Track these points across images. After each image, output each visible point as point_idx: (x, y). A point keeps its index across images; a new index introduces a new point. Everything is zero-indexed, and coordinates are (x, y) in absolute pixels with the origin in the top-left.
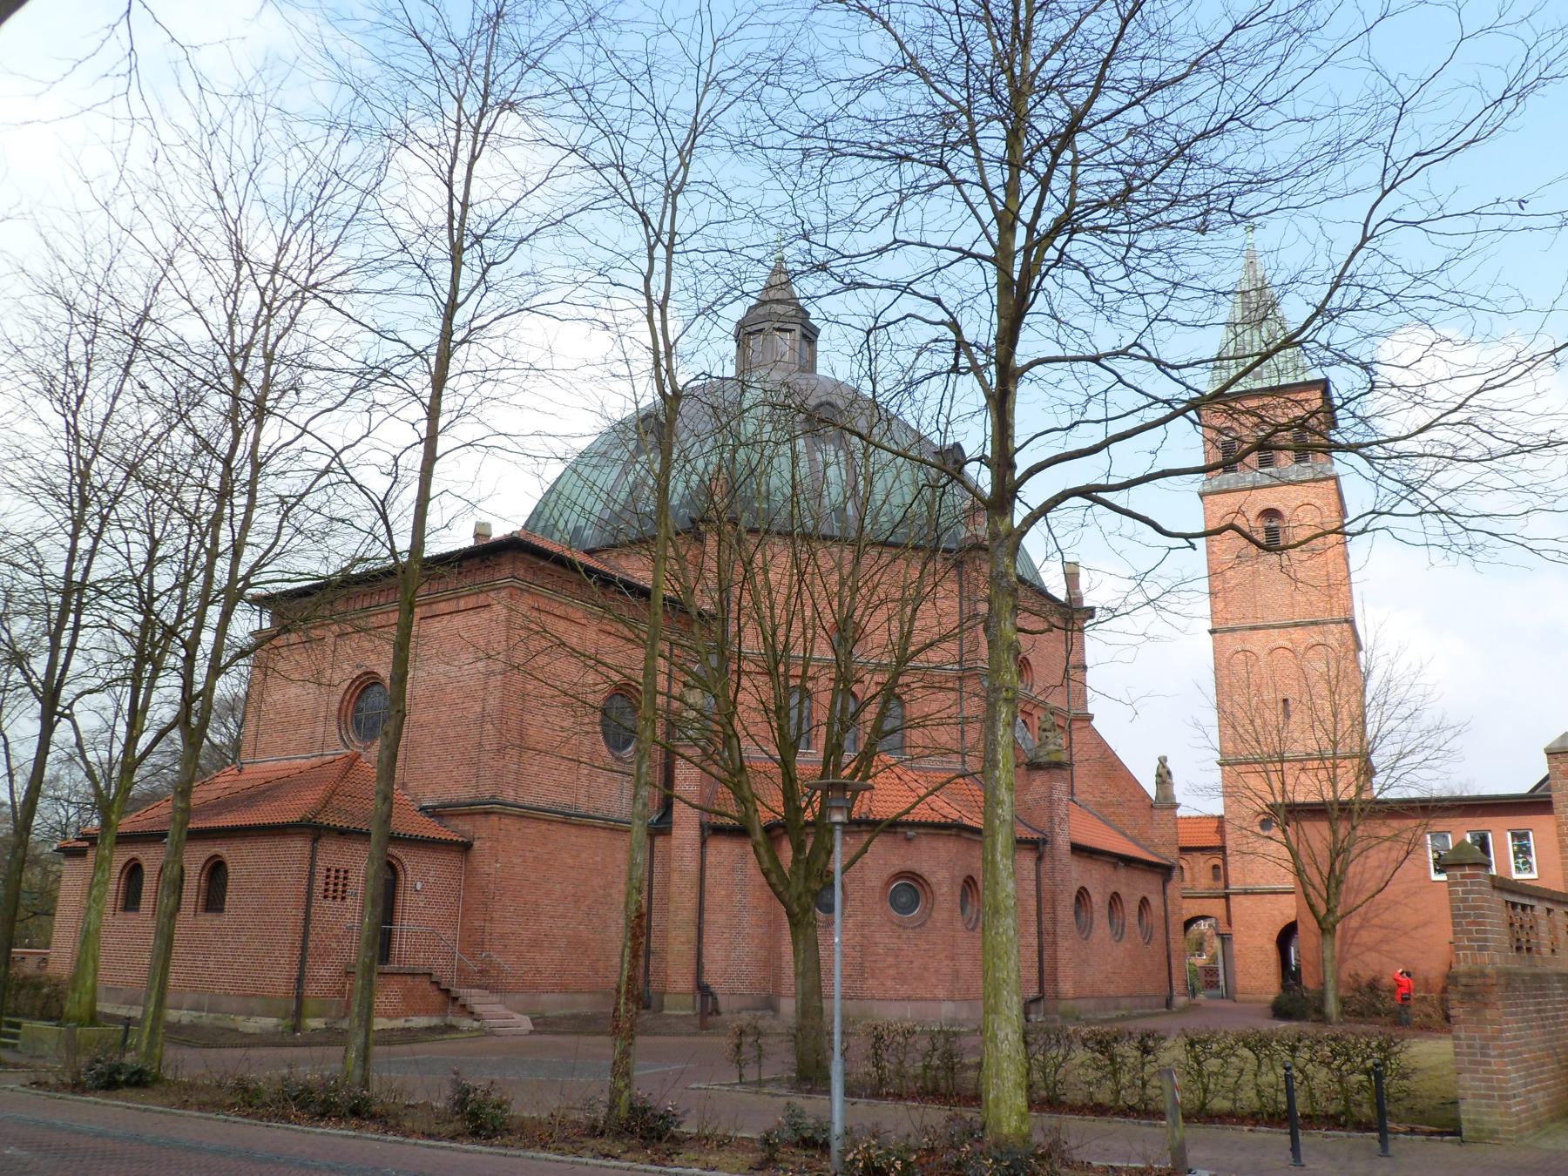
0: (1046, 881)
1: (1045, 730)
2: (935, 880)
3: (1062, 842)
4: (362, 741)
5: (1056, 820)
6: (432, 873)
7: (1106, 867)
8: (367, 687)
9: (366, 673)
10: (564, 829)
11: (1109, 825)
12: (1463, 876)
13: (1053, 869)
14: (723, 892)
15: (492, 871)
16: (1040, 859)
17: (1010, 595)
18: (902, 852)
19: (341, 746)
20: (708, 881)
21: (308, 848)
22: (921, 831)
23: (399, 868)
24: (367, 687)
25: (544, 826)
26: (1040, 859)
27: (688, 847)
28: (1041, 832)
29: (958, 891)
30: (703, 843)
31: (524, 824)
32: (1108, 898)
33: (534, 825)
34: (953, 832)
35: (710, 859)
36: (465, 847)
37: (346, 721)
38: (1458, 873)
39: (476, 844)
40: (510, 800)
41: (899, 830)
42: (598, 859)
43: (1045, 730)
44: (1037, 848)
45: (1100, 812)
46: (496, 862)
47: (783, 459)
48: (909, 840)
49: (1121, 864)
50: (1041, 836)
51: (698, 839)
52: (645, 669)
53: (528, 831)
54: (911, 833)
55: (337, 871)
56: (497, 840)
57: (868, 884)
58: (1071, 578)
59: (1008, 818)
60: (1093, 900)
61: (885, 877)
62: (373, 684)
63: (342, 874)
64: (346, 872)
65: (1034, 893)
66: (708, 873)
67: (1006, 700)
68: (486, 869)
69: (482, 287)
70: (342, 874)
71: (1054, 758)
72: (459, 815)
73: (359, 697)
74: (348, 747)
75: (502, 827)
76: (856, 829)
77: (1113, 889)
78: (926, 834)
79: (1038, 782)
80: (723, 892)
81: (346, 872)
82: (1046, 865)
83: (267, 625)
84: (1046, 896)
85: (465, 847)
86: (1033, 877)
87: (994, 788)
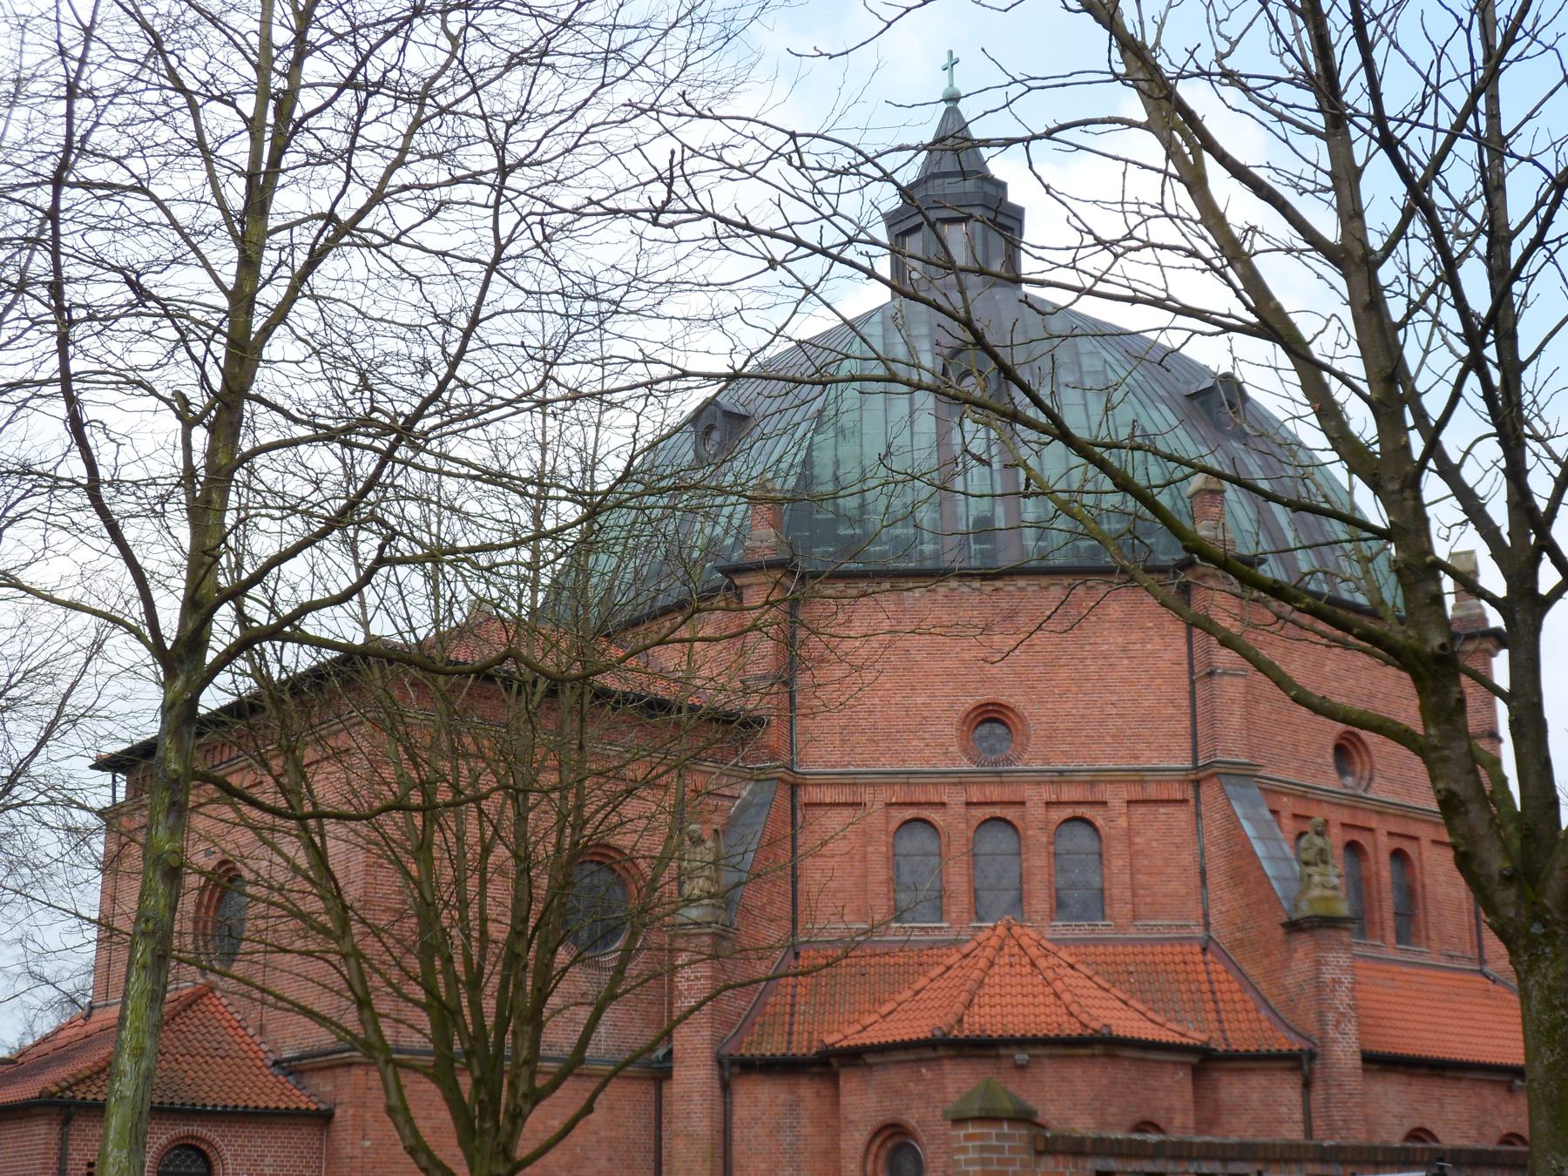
1: (1307, 863)
3: (1344, 1050)
5: (1331, 1017)
6: (268, 1160)
7: (1487, 1091)
12: (968, 1137)
13: (1327, 1100)
14: (763, 1166)
15: (358, 1152)
16: (1307, 1085)
17: (168, 789)
20: (738, 1148)
21: (54, 1136)
22: (1039, 1051)
23: (212, 1155)
26: (1307, 1085)
27: (696, 1097)
28: (1308, 1039)
30: (726, 1088)
34: (1098, 1050)
35: (740, 1113)
36: (323, 1118)
38: (994, 1132)
39: (338, 1112)
41: (1003, 1051)
43: (1307, 863)
44: (1297, 1069)
46: (364, 1138)
47: (658, 415)
48: (1021, 1067)
50: (1306, 1046)
51: (717, 1084)
54: (1021, 1057)
56: (363, 1105)
59: (129, 1093)
66: (737, 1135)
68: (348, 1150)
69: (835, 219)
71: (1321, 910)
72: (320, 1069)
73: (220, 899)
76: (932, 1055)
78: (1051, 1057)
79: (1299, 955)
80: (763, 1166)
82: (1317, 1096)
83: (121, 795)
85: (323, 1118)
86: (1298, 1116)
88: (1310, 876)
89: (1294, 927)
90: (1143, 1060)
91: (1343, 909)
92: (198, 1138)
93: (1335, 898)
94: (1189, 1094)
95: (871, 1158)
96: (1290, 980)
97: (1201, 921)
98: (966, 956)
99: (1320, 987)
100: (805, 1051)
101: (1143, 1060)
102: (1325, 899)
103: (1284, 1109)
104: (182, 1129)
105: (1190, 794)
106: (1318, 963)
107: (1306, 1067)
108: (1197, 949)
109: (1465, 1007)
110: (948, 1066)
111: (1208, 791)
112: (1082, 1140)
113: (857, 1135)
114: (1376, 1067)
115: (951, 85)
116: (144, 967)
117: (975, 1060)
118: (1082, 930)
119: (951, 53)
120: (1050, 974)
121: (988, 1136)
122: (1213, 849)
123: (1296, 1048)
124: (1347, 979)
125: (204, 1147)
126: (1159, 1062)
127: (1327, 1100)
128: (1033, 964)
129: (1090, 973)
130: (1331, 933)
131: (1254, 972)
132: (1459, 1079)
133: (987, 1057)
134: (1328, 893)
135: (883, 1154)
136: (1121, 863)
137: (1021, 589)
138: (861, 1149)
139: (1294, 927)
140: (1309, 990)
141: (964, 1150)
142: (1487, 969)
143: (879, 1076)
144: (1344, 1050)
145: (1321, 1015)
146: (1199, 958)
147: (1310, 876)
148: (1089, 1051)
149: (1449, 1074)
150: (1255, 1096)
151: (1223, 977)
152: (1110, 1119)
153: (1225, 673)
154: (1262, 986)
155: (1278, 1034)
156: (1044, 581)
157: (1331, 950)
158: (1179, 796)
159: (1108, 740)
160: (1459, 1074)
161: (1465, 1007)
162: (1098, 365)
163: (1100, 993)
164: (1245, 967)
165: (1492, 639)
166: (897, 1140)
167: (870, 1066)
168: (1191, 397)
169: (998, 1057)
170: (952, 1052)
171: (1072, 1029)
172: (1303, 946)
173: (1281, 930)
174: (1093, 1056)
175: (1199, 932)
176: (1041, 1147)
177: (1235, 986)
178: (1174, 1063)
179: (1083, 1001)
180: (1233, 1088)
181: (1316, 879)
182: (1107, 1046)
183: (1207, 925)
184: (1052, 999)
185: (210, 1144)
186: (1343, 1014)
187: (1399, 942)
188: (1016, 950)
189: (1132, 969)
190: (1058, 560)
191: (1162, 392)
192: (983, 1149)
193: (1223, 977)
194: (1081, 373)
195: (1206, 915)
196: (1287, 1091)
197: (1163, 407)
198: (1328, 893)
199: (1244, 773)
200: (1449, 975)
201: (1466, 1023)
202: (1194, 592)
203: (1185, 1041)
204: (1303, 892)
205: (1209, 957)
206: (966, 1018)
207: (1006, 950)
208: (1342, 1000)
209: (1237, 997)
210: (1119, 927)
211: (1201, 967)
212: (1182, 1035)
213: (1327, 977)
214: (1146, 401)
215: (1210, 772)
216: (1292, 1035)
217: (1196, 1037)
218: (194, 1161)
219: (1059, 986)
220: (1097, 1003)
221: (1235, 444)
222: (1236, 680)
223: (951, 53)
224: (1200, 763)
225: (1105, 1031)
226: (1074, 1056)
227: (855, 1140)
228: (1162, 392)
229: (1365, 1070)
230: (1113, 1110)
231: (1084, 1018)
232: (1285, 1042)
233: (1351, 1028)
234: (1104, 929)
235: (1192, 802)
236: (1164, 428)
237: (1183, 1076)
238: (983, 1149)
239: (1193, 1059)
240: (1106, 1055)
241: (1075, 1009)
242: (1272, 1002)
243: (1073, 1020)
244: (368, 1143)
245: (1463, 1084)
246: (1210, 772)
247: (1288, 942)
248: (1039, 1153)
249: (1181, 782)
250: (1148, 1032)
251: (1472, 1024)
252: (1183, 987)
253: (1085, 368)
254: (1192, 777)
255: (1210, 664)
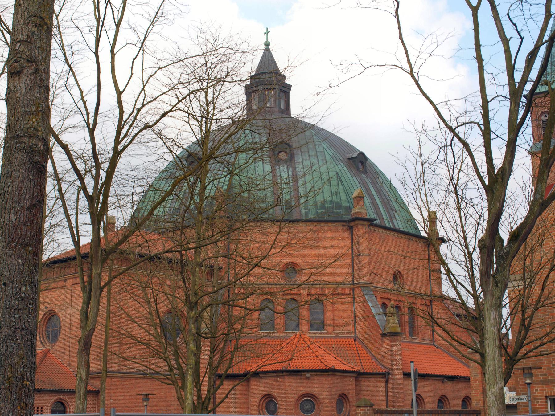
0: (390, 393)
2: (321, 397)
3: (398, 372)
4: (51, 343)
5: (394, 362)
7: (436, 383)
8: (50, 318)
9: (50, 310)
10: (144, 381)
11: (454, 357)
12: (361, 410)
14: (225, 406)
15: (109, 403)
16: (387, 382)
17: (193, 336)
18: (305, 384)
19: (41, 345)
22: (313, 373)
23: (66, 404)
24: (50, 318)
25: (133, 381)
26: (387, 382)
29: (334, 402)
31: (124, 380)
32: (437, 399)
33: (128, 381)
34: (330, 373)
37: (43, 337)
40: (116, 370)
41: (303, 374)
42: (163, 394)
45: (448, 350)
48: (308, 378)
49: (445, 380)
50: (387, 370)
52: (104, 354)
53: (126, 383)
54: (308, 375)
55: (38, 408)
57: (288, 400)
58: (432, 219)
59: (190, 402)
60: (426, 400)
61: (296, 397)
62: (53, 316)
63: (40, 409)
64: (42, 408)
65: (384, 399)
67: (190, 368)
70: (40, 409)
71: (393, 331)
72: (94, 378)
73: (47, 322)
74: (44, 346)
75: (113, 383)
76: (282, 374)
77: (441, 393)
78: (316, 375)
79: (386, 343)
81: (42, 408)
82: (390, 385)
84: (390, 401)
86: (384, 391)
87: (186, 394)
88: (389, 320)
89: (384, 335)
90: (342, 376)
91: (399, 330)
92: (62, 399)
93: (397, 327)
94: (354, 386)
95: (261, 404)
96: (382, 351)
97: (354, 331)
98: (287, 344)
99: (392, 353)
100: (238, 372)
101: (342, 376)
102: (394, 327)
103: (380, 389)
104: (58, 397)
105: (351, 292)
106: (391, 346)
107: (387, 377)
108: (353, 340)
109: (429, 356)
110: (286, 378)
111: (357, 291)
112: (383, 410)
113: (256, 398)
114: (406, 376)
115: (267, 40)
116: (191, 375)
117: (294, 376)
118: (317, 334)
119: (267, 29)
120: (314, 350)
121: (365, 410)
122: (358, 309)
123: (384, 371)
124: (399, 351)
125: (64, 402)
126: (346, 376)
127: (393, 387)
128: (308, 346)
129: (325, 349)
130: (395, 337)
131: (371, 348)
132: (429, 379)
133: (298, 375)
134: (395, 325)
135: (265, 403)
136: (330, 313)
137: (301, 226)
138: (258, 402)
139: (384, 335)
140: (388, 354)
141: (360, 413)
142: (435, 344)
143: (264, 380)
144: (398, 372)
145: (392, 361)
146: (353, 342)
147: (389, 320)
148: (328, 373)
149: (426, 378)
150: (372, 385)
151: (361, 349)
152: (333, 393)
153: (363, 255)
154: (373, 352)
155: (378, 367)
156: (308, 224)
157: (395, 342)
158: (348, 293)
159: (327, 275)
160: (429, 378)
161: (429, 356)
162: (322, 149)
163: (328, 355)
164: (368, 346)
165: (440, 240)
166: (269, 399)
167: (261, 377)
168: (349, 159)
169: (301, 375)
170: (288, 374)
171: (323, 367)
172: (387, 340)
173: (380, 336)
174: (329, 375)
175: (353, 335)
176: (375, 412)
177: (365, 352)
178: (350, 376)
179: (325, 358)
180: (366, 383)
181: (391, 321)
182: (333, 372)
183: (356, 332)
184: (315, 358)
185: (65, 401)
186: (398, 361)
187: (409, 336)
188: (303, 342)
189: (333, 346)
190: (311, 216)
191: (341, 158)
192: (364, 413)
193: (361, 349)
194: (316, 152)
195: (355, 329)
196: (381, 384)
197: (342, 164)
198: (395, 325)
199: (367, 286)
200: (424, 346)
201: (430, 362)
202: (354, 229)
203: (354, 370)
204: (387, 325)
205: (356, 342)
206: (291, 363)
207: (300, 342)
208: (398, 357)
209: (365, 355)
210: (329, 333)
211: (354, 346)
212: (352, 368)
213: (394, 350)
214: (337, 162)
215: (358, 286)
216: (383, 367)
217: (357, 368)
218: (60, 406)
219: (317, 353)
220: (328, 358)
221: (363, 176)
222: (366, 257)
223: (267, 29)
224: (354, 283)
225: (333, 367)
226: (323, 375)
227: (255, 399)
228: (341, 158)
229: (403, 377)
230: (334, 390)
231: (326, 364)
232: (383, 370)
233: (400, 365)
234: (324, 333)
235: (352, 294)
236: (324, 142)
237: (352, 380)
238: (364, 413)
239: (355, 375)
240: (332, 375)
241: (323, 360)
242: (376, 357)
243: (322, 364)
244: (112, 400)
245: (430, 381)
246: (358, 286)
247: (382, 339)
248: (375, 413)
249: (349, 288)
250: (343, 367)
251: (432, 362)
252: (349, 352)
253: (318, 150)
254: (352, 287)
255: (359, 252)
